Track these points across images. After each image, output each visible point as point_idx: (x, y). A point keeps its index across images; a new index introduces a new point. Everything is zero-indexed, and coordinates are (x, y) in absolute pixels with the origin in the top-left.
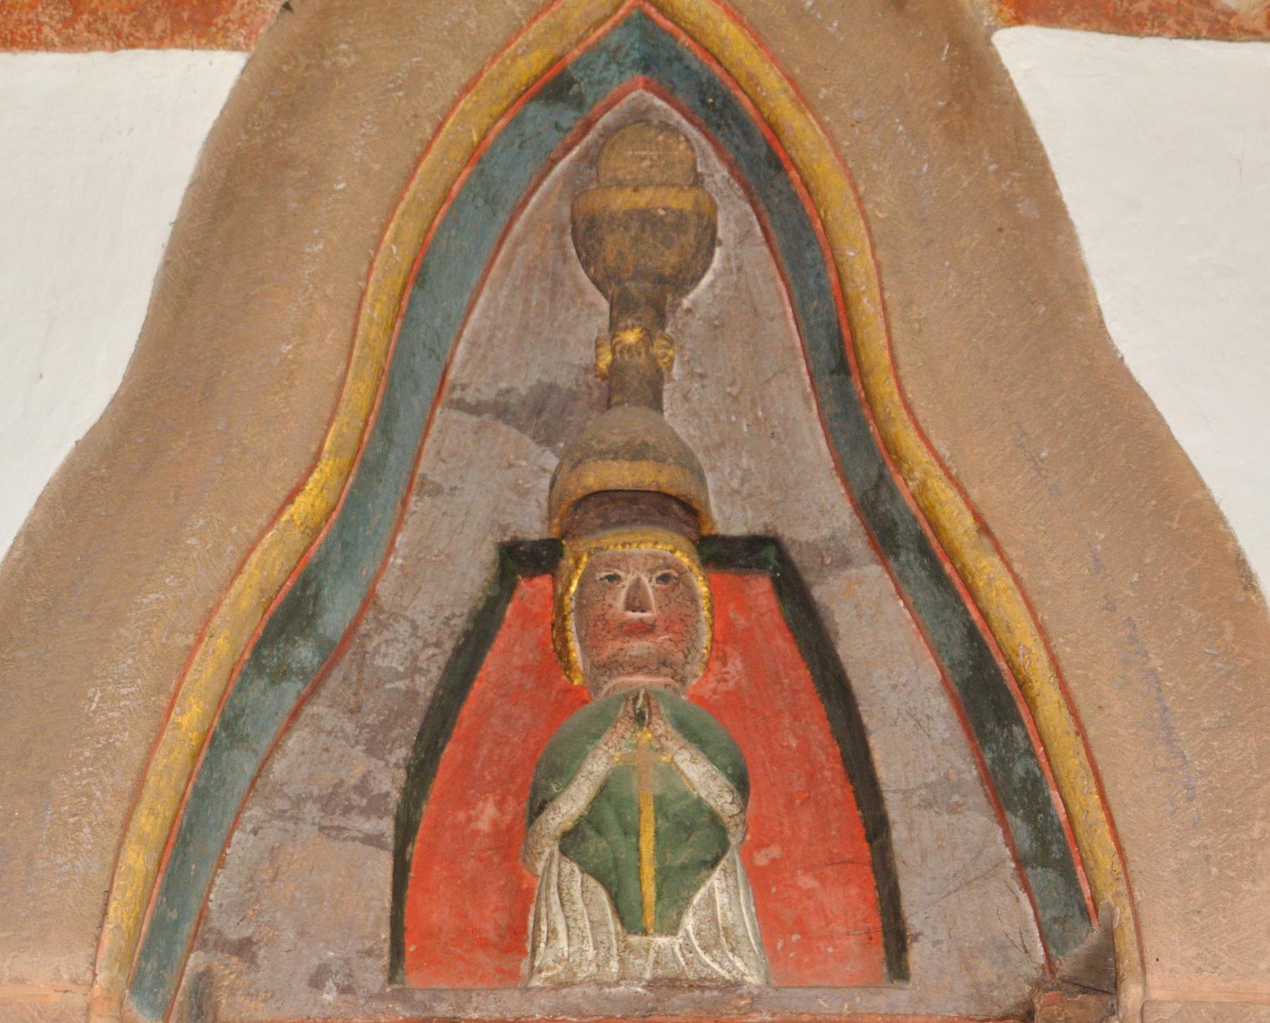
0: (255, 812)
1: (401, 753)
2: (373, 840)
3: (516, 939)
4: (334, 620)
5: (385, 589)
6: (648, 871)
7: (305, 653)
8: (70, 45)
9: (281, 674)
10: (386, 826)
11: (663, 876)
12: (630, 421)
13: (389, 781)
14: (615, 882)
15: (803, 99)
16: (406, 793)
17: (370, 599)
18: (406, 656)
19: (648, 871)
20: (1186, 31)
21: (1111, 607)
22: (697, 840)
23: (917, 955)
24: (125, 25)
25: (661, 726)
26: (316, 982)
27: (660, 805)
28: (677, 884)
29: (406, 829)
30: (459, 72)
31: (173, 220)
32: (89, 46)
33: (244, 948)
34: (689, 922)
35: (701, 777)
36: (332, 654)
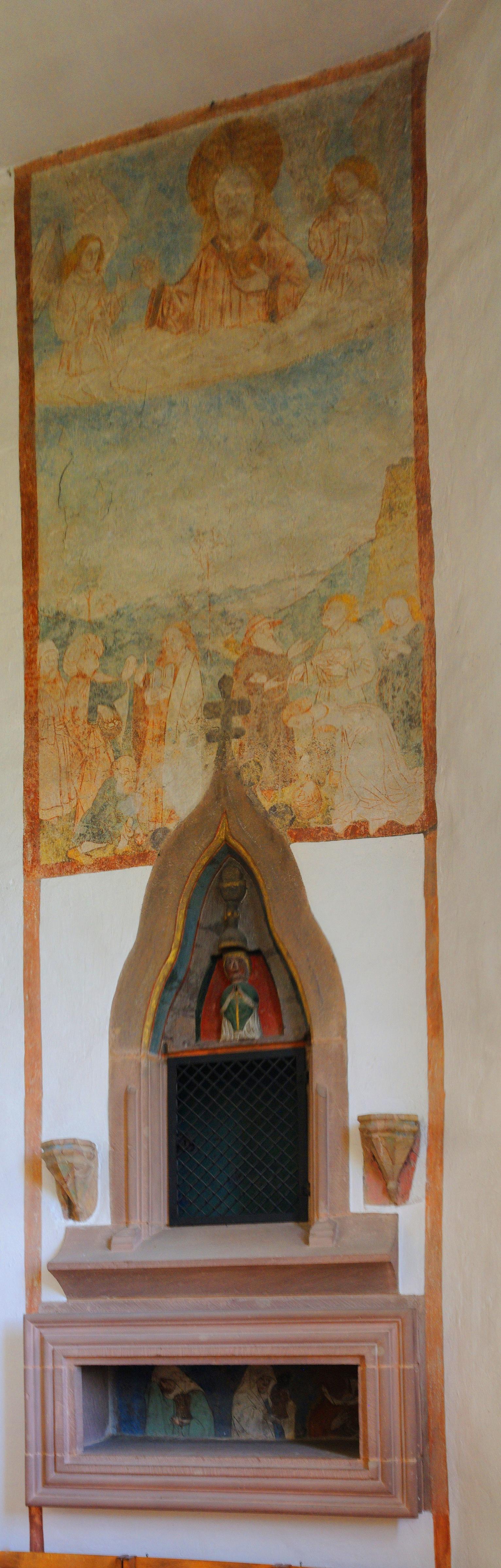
0: (171, 1013)
1: (195, 999)
2: (192, 1017)
3: (219, 1031)
4: (181, 975)
5: (191, 967)
6: (238, 1019)
7: (176, 984)
8: (121, 868)
9: (171, 989)
10: (194, 1014)
11: (240, 1020)
12: (229, 932)
13: (194, 1005)
14: (232, 1022)
15: (255, 864)
16: (198, 1007)
17: (188, 970)
18: (196, 980)
19: (238, 1019)
20: (328, 840)
21: (310, 967)
22: (246, 1012)
23: (285, 1030)
24: (130, 861)
25: (240, 990)
26: (184, 1043)
27: (240, 1007)
28: (243, 1022)
29: (198, 1013)
30: (191, 865)
31: (150, 1556)
32: (125, 868)
33: (171, 1039)
34: (245, 1028)
35: (247, 1000)
36: (182, 983)
